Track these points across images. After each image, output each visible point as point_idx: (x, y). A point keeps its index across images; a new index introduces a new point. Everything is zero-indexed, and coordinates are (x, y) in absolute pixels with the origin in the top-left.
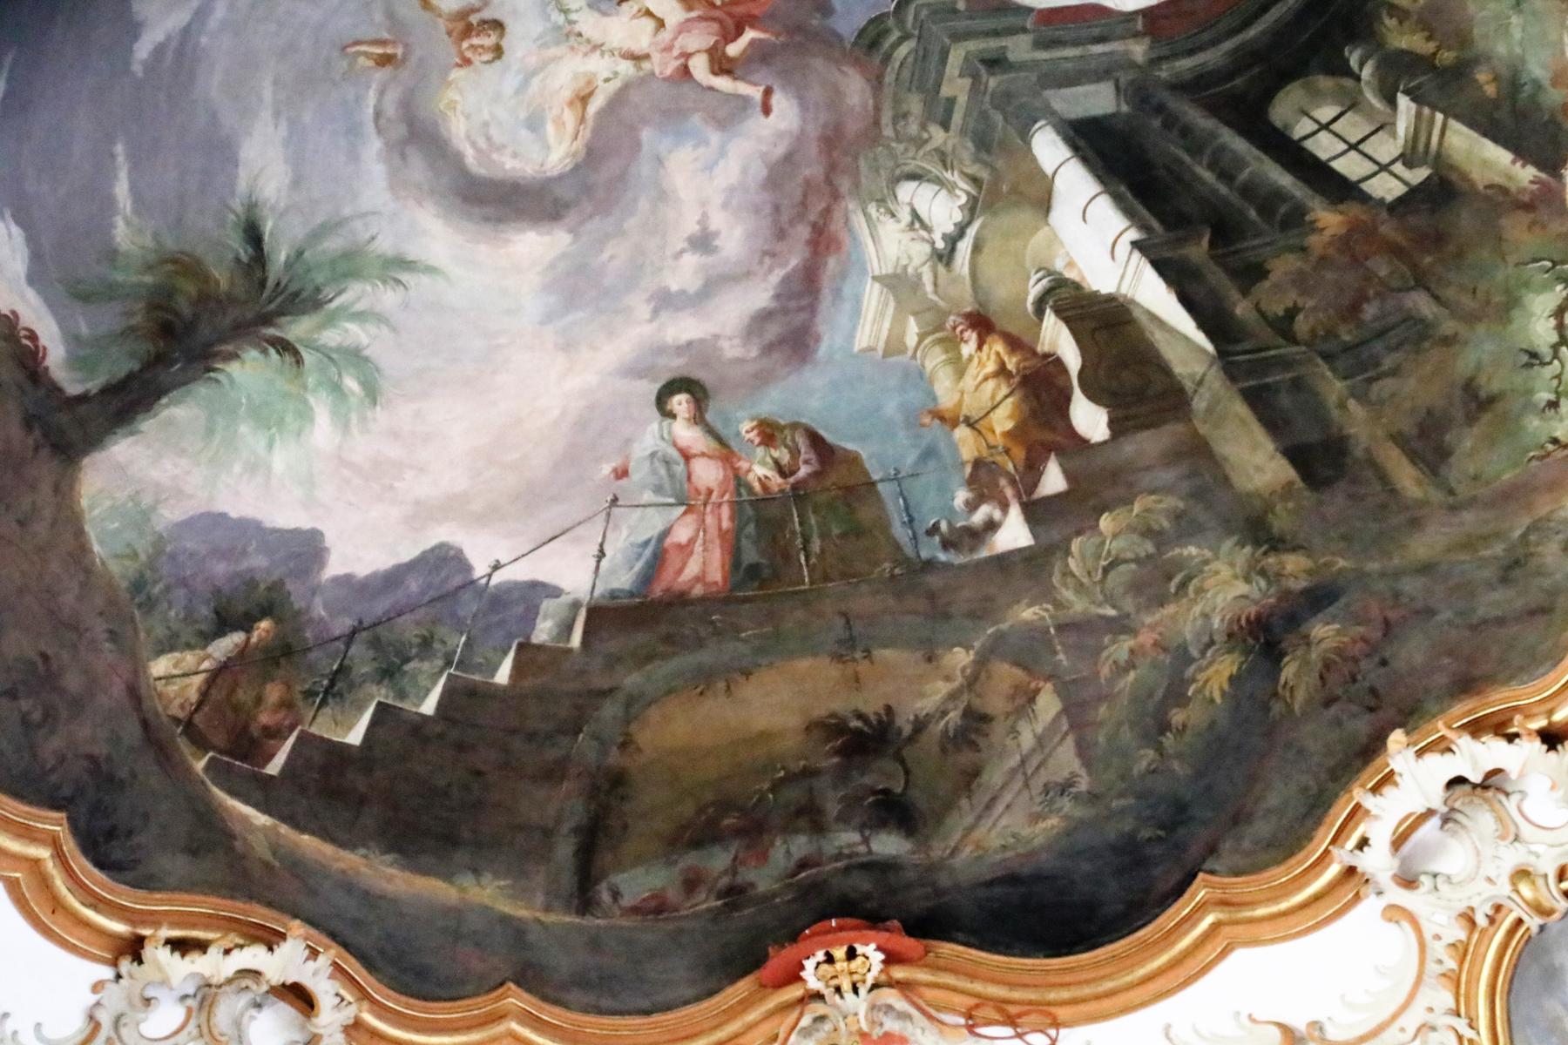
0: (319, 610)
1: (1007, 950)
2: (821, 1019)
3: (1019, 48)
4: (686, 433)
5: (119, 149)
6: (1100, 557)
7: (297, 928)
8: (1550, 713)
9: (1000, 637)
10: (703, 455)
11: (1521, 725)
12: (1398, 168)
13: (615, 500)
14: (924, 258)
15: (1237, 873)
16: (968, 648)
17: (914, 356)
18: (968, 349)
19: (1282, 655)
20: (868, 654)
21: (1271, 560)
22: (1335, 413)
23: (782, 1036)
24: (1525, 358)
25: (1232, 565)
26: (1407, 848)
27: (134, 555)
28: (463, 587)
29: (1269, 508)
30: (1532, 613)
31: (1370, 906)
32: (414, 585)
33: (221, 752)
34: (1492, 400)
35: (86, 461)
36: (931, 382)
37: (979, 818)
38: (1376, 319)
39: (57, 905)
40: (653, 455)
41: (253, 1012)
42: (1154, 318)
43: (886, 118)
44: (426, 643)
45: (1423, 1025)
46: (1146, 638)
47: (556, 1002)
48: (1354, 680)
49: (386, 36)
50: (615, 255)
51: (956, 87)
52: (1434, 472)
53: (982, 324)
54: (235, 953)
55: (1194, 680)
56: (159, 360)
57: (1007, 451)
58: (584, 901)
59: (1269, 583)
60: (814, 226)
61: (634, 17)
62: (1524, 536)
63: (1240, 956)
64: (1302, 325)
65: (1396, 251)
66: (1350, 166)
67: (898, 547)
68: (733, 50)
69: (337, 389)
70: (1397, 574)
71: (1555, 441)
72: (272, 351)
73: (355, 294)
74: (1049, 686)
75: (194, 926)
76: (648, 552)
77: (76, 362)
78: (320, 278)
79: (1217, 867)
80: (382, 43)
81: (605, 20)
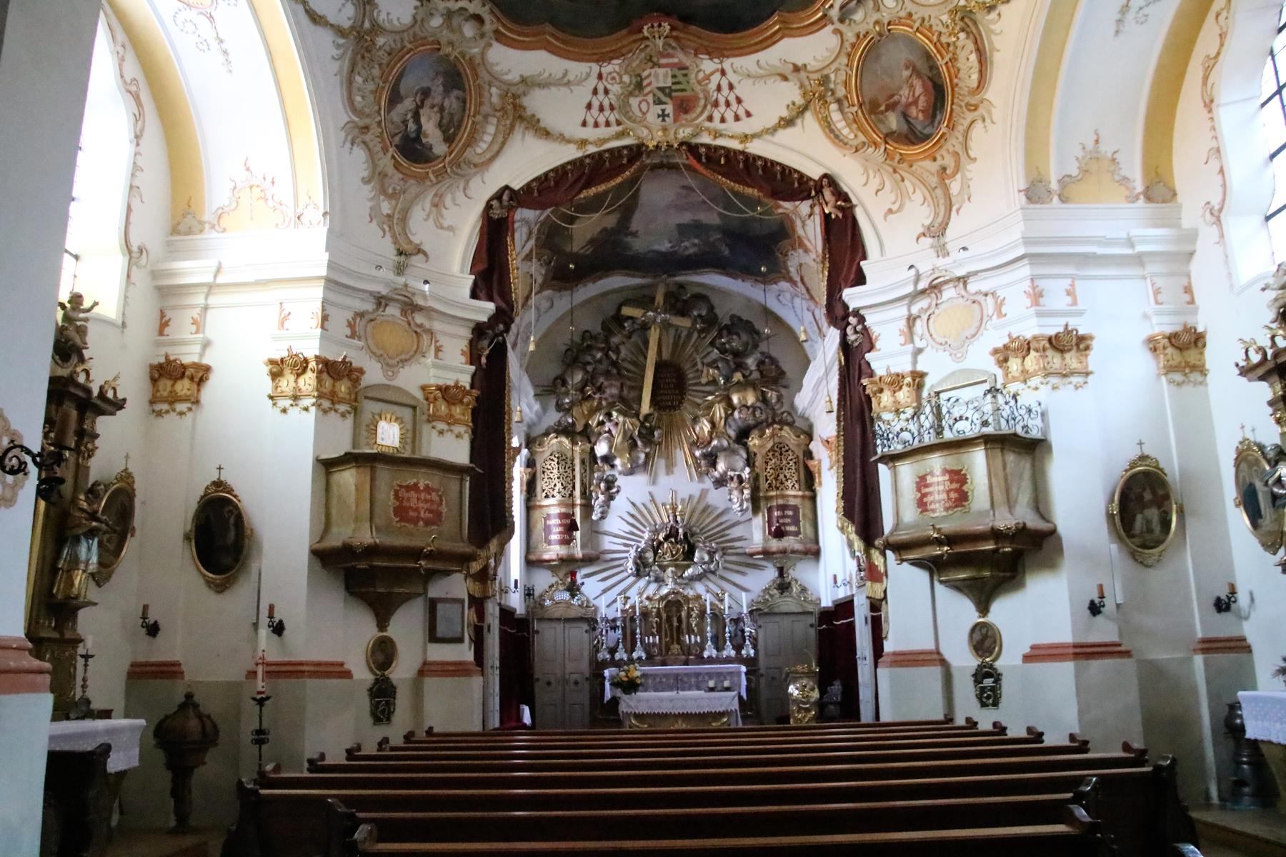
1: (711, 30)
31: (829, 28)
47: (563, 32)
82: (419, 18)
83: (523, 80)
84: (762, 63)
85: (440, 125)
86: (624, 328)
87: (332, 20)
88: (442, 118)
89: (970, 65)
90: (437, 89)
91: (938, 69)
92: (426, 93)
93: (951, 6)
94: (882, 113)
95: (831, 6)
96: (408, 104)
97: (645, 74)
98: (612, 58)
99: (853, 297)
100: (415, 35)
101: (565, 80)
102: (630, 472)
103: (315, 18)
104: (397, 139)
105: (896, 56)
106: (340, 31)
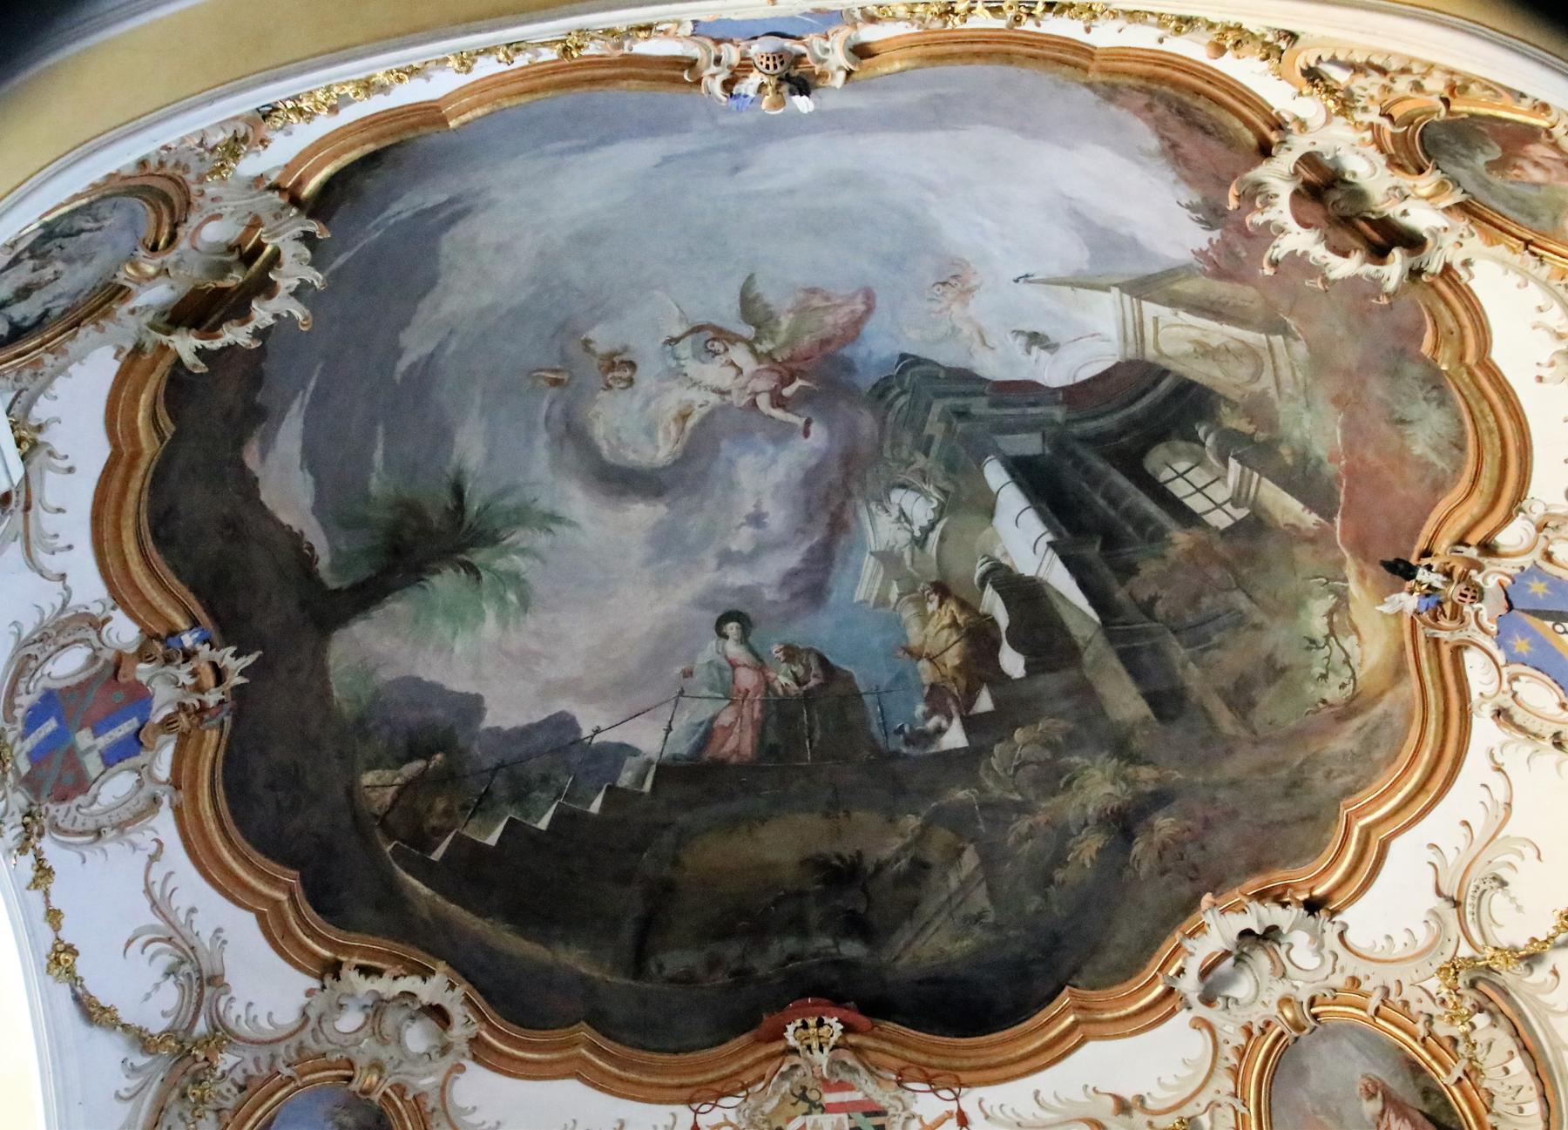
0: (476, 749)
1: (929, 1030)
2: (795, 1067)
3: (979, 406)
4: (733, 649)
5: (380, 429)
6: (1013, 758)
7: (441, 967)
8: (1312, 889)
9: (939, 811)
10: (745, 665)
11: (1292, 896)
12: (1228, 507)
13: (682, 693)
14: (904, 543)
16: (917, 814)
17: (894, 609)
18: (932, 607)
19: (1134, 837)
20: (848, 814)
21: (1130, 770)
22: (1179, 671)
23: (767, 1077)
24: (1307, 643)
25: (1103, 771)
26: (1210, 978)
27: (359, 701)
28: (573, 743)
29: (1131, 733)
30: (1303, 819)
31: (1183, 1017)
32: (541, 738)
33: (404, 841)
34: (1283, 670)
35: (336, 634)
36: (905, 627)
37: (916, 936)
38: (1208, 608)
39: (287, 932)
40: (710, 663)
41: (408, 1022)
42: (1061, 596)
43: (887, 444)
44: (545, 779)
45: (1212, 1102)
46: (1041, 818)
48: (1182, 859)
49: (558, 367)
50: (695, 525)
51: (934, 428)
52: (1244, 717)
53: (942, 590)
54: (401, 979)
55: (1072, 850)
56: (388, 571)
57: (954, 680)
59: (1128, 785)
60: (833, 515)
61: (723, 366)
62: (1302, 764)
63: (1091, 1048)
64: (1160, 609)
65: (1225, 563)
66: (1197, 504)
67: (874, 741)
68: (787, 392)
69: (502, 600)
70: (1217, 786)
71: (1324, 701)
72: (462, 571)
73: (520, 536)
74: (972, 847)
75: (375, 959)
76: (702, 729)
77: (334, 567)
78: (498, 523)
79: (1079, 983)
80: (556, 371)
81: (704, 367)
84: (1046, 1096)
87: (126, 1016)
89: (1515, 1083)
91: (1441, 1094)
93: (1440, 961)
95: (1181, 971)
100: (301, 1048)
103: (91, 1011)
106: (142, 1040)
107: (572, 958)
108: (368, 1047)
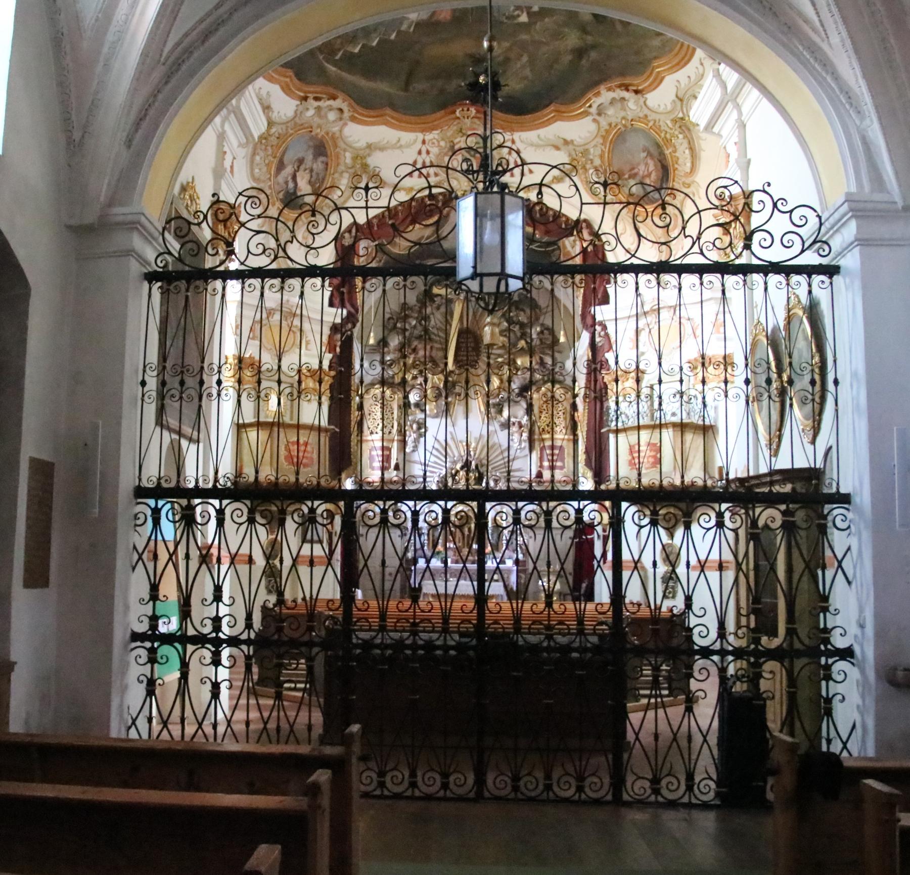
15: (562, 104)
58: (406, 89)
82: (298, 112)
83: (369, 146)
84: (542, 136)
85: (310, 182)
86: (434, 301)
88: (311, 176)
90: (309, 157)
92: (301, 161)
93: (673, 116)
94: (626, 179)
96: (289, 170)
97: (456, 141)
98: (433, 130)
99: (602, 313)
100: (296, 124)
101: (398, 145)
102: (436, 416)
104: (281, 196)
105: (636, 143)
107: (383, 86)
108: (316, 119)
